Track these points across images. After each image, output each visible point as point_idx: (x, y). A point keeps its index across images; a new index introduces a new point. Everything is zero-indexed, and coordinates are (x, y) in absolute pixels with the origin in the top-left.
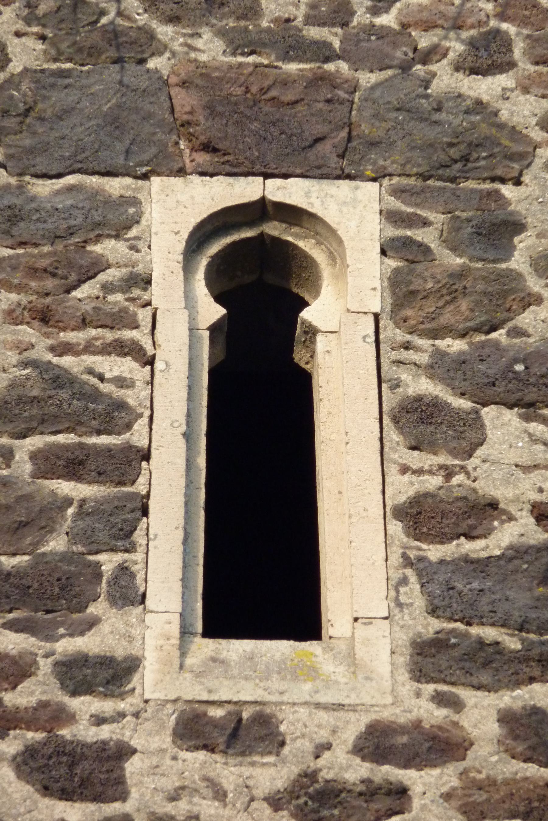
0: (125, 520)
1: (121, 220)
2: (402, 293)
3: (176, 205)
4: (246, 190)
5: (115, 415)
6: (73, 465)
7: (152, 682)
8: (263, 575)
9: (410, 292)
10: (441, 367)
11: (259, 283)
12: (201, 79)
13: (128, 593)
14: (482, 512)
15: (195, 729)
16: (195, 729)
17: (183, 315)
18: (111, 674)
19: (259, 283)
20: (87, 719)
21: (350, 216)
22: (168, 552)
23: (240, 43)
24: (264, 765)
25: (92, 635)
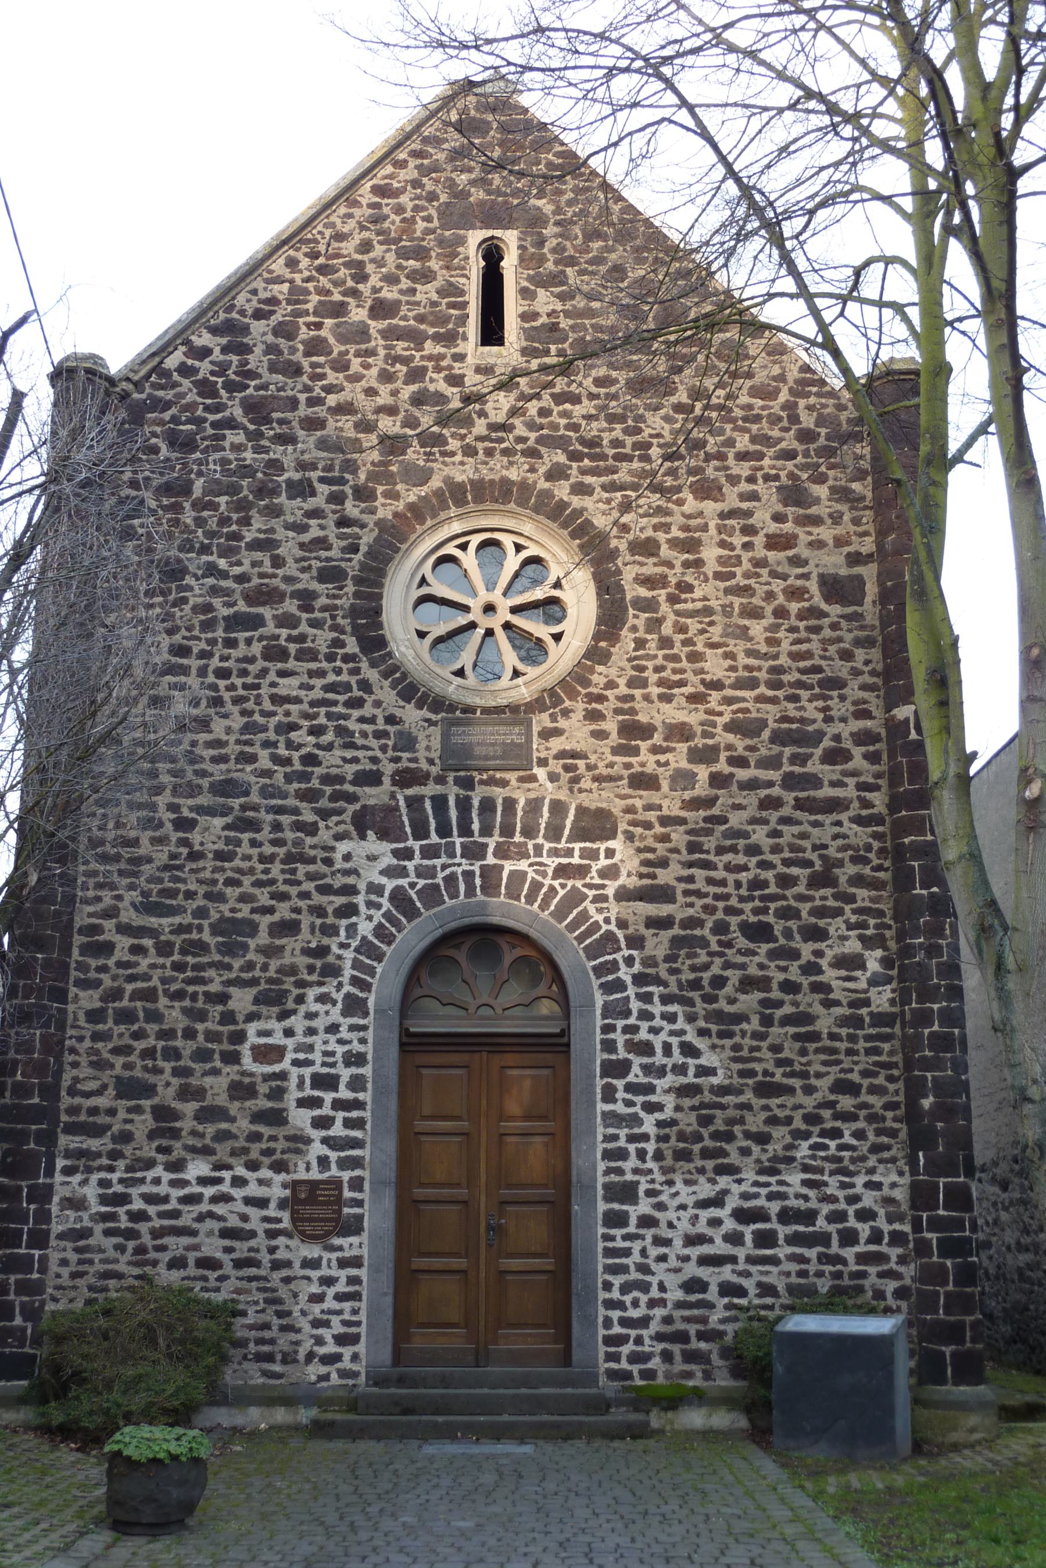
0: (463, 320)
1: (462, 241)
2: (522, 259)
3: (475, 237)
4: (489, 233)
5: (462, 293)
6: (452, 306)
7: (470, 360)
8: (492, 332)
9: (523, 260)
10: (530, 279)
11: (492, 255)
12: (481, 203)
13: (465, 338)
14: (535, 315)
15: (478, 370)
16: (478, 370)
17: (476, 266)
18: (460, 358)
19: (492, 255)
20: (458, 368)
21: (510, 239)
22: (473, 328)
23: (489, 193)
24: (799, 183)
25: (851, 1506)
